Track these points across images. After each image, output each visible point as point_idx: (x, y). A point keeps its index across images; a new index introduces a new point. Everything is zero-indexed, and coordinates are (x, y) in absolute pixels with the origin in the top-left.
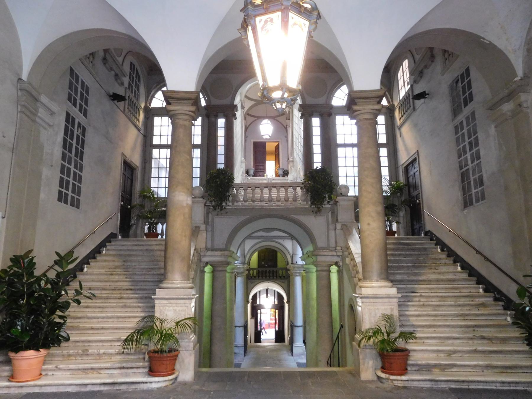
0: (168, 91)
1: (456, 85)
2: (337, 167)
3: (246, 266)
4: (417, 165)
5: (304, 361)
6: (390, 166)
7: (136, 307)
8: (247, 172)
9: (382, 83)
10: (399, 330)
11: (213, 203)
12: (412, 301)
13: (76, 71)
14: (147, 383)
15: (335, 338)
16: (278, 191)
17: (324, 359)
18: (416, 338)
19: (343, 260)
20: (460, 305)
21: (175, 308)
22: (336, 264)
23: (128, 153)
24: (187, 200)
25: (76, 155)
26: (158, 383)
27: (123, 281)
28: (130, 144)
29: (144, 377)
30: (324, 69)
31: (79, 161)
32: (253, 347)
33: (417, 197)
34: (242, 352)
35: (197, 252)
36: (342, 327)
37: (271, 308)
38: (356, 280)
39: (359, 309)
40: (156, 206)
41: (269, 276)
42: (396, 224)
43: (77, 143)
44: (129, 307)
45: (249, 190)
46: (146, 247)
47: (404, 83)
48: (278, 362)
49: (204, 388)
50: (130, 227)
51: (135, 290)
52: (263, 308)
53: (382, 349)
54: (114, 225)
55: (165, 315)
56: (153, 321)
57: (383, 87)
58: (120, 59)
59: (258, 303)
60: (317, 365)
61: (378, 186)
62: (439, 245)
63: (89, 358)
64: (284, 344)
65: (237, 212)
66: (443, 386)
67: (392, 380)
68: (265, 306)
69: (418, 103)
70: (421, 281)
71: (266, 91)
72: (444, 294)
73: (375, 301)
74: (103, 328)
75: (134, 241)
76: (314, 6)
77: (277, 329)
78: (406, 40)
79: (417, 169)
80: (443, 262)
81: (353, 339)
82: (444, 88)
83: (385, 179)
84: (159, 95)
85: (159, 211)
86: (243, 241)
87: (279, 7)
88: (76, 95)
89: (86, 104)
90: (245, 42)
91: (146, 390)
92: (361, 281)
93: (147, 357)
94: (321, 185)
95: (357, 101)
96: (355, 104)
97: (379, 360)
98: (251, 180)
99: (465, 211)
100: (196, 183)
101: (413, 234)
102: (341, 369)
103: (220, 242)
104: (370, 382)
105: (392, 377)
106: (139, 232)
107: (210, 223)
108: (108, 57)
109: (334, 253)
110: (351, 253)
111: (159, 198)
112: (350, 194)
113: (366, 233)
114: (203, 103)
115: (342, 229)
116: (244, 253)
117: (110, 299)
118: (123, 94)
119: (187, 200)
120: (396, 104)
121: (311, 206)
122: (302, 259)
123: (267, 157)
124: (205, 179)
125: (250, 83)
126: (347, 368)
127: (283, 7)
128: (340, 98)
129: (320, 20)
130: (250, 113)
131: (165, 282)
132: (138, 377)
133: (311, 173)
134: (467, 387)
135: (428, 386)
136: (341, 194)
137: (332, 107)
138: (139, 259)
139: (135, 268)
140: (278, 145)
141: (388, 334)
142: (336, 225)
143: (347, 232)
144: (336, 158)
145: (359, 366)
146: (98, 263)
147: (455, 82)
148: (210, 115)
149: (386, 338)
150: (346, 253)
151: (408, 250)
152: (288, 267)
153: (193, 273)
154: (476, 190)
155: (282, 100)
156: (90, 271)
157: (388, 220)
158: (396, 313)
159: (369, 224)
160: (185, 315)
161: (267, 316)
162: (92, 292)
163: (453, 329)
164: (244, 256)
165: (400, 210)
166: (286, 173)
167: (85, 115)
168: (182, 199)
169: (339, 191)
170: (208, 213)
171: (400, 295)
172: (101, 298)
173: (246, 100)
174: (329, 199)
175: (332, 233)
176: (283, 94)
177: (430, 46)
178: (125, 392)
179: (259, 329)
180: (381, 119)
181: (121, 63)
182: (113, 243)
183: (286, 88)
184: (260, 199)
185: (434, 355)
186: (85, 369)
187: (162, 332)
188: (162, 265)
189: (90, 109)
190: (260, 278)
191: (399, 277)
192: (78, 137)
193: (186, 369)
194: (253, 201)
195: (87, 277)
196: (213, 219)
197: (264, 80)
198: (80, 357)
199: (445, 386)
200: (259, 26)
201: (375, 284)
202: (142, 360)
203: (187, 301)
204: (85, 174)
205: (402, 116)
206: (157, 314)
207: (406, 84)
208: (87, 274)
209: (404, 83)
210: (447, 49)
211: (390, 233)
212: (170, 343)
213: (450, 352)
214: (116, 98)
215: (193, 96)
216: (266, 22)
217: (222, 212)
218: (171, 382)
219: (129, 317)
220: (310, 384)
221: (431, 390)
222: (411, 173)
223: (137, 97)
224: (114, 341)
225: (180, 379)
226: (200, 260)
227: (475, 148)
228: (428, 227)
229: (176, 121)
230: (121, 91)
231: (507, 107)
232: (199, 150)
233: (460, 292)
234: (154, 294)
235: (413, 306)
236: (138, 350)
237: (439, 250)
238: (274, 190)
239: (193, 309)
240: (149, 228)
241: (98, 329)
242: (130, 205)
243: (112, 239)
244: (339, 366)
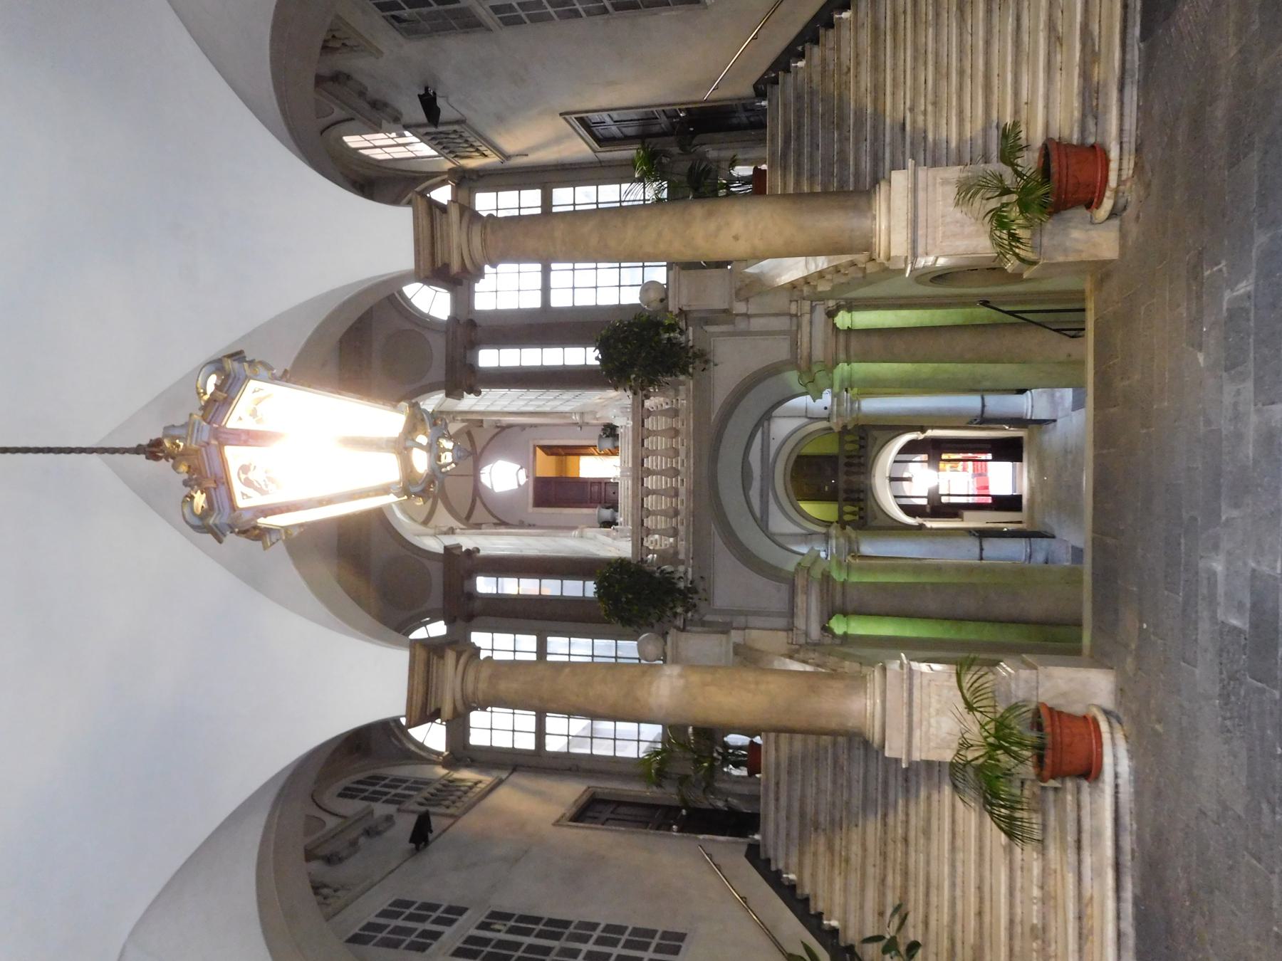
0: (408, 715)
1: (405, 21)
2: (597, 309)
3: (833, 531)
4: (595, 117)
5: (1068, 394)
6: (597, 181)
7: (929, 805)
8: (608, 524)
9: (395, 201)
10: (996, 166)
11: (679, 610)
12: (925, 132)
13: (356, 930)
14: (1117, 786)
15: (1012, 319)
16: (654, 453)
17: (1067, 346)
18: (1016, 124)
19: (822, 298)
20: (937, 15)
21: (932, 711)
22: (831, 314)
23: (556, 811)
24: (670, 676)
25: (557, 936)
26: (1117, 759)
27: (864, 832)
28: (534, 805)
29: (1103, 791)
30: (366, 345)
31: (571, 929)
32: (1031, 517)
33: (672, 115)
34: (1044, 543)
35: (797, 651)
36: (985, 303)
37: (938, 470)
38: (871, 268)
39: (942, 262)
40: (684, 746)
42: (737, 168)
43: (527, 932)
44: (928, 821)
45: (650, 502)
46: (784, 777)
47: (398, 145)
48: (1070, 457)
49: (1133, 646)
50: (732, 812)
51: (886, 806)
52: (937, 488)
53: (1043, 206)
54: (728, 849)
55: (949, 737)
56: (964, 765)
57: (405, 200)
58: (331, 822)
59: (924, 502)
60: (1081, 363)
61: (644, 214)
62: (789, 66)
63: (1053, 923)
64: (1025, 440)
65: (700, 552)
66: (1135, 56)
67: (1120, 182)
68: (932, 484)
69: (446, 113)
70: (875, 109)
71: (410, 486)
72: (909, 53)
73: (924, 222)
74: (980, 888)
75: (766, 804)
76: (212, 367)
77: (989, 456)
78: (298, 146)
79: (605, 116)
80: (829, 54)
81: (1017, 277)
82: (414, 49)
83: (627, 193)
84: (418, 733)
85: (694, 744)
86: (771, 537)
87: (214, 451)
88: (412, 931)
90: (295, 533)
91: (1135, 788)
92: (875, 256)
93: (1052, 783)
94: (639, 349)
96: (446, 266)
97: (1068, 214)
98: (624, 515)
100: (629, 648)
102: (1090, 306)
103: (773, 595)
104: (1123, 235)
105: (1113, 181)
106: (745, 790)
107: (728, 619)
108: (326, 850)
109: (806, 318)
110: (806, 280)
111: (665, 739)
112: (663, 280)
114: (438, 629)
115: (747, 300)
116: (802, 535)
118: (413, 819)
119: (670, 676)
120: (448, 165)
121: (691, 375)
122: (817, 396)
123: (571, 474)
124: (618, 627)
126: (1088, 293)
127: (214, 442)
128: (433, 302)
129: (246, 354)
130: (464, 516)
131: (868, 735)
132: (1102, 806)
133: (610, 374)
135: (1135, 93)
136: (662, 300)
137: (453, 319)
138: (811, 792)
139: (834, 804)
140: (543, 448)
141: (1006, 191)
143: (753, 288)
144: (574, 310)
145: (1082, 262)
146: (820, 892)
147: (396, 24)
148: (470, 612)
149: (1014, 197)
150: (806, 289)
151: (799, 138)
152: (837, 429)
153: (847, 663)
155: (434, 450)
156: (837, 911)
157: (727, 187)
158: (954, 173)
159: (736, 238)
160: (950, 688)
161: (955, 480)
162: (889, 911)
163: (996, 30)
164: (807, 537)
165: (703, 157)
166: (610, 431)
167: (461, 911)
168: (667, 687)
169: (656, 305)
170: (703, 624)
171: (910, 162)
172: (905, 889)
173: (432, 523)
174: (674, 331)
175: (756, 324)
176: (420, 446)
177: (312, 80)
178: (1140, 839)
179: (989, 500)
180: (485, 202)
181: (340, 820)
182: (771, 854)
183: (406, 439)
184: (671, 497)
185: (1059, 79)
187: (990, 744)
188: (826, 740)
189: (446, 900)
191: (866, 164)
192: (512, 931)
193: (1085, 687)
194: (676, 513)
195: (853, 920)
196: (721, 612)
197: (385, 490)
199: (1136, 52)
200: (256, 500)
201: (881, 223)
202: (1060, 795)
203: (916, 681)
204: (603, 917)
205: (477, 150)
206: (948, 756)
207: (401, 140)
208: (845, 921)
209: (398, 145)
210: (320, 44)
211: (758, 183)
212: (1020, 727)
213: (1053, 39)
214: (421, 835)
215: (421, 654)
216: (248, 483)
217: (700, 589)
218: (1116, 725)
219: (953, 822)
220: (1126, 383)
221: (1145, 87)
222: (614, 130)
223: (419, 784)
225: (1108, 703)
226: (816, 646)
228: (744, 88)
229: (480, 696)
230: (406, 824)
232: (549, 639)
233: (905, 12)
234: (897, 761)
235: (936, 126)
236: (1034, 805)
237: (801, 64)
238: (649, 463)
239: (936, 667)
240: (737, 766)
241: (981, 900)
242: (679, 809)
243: (763, 856)
244: (1083, 310)
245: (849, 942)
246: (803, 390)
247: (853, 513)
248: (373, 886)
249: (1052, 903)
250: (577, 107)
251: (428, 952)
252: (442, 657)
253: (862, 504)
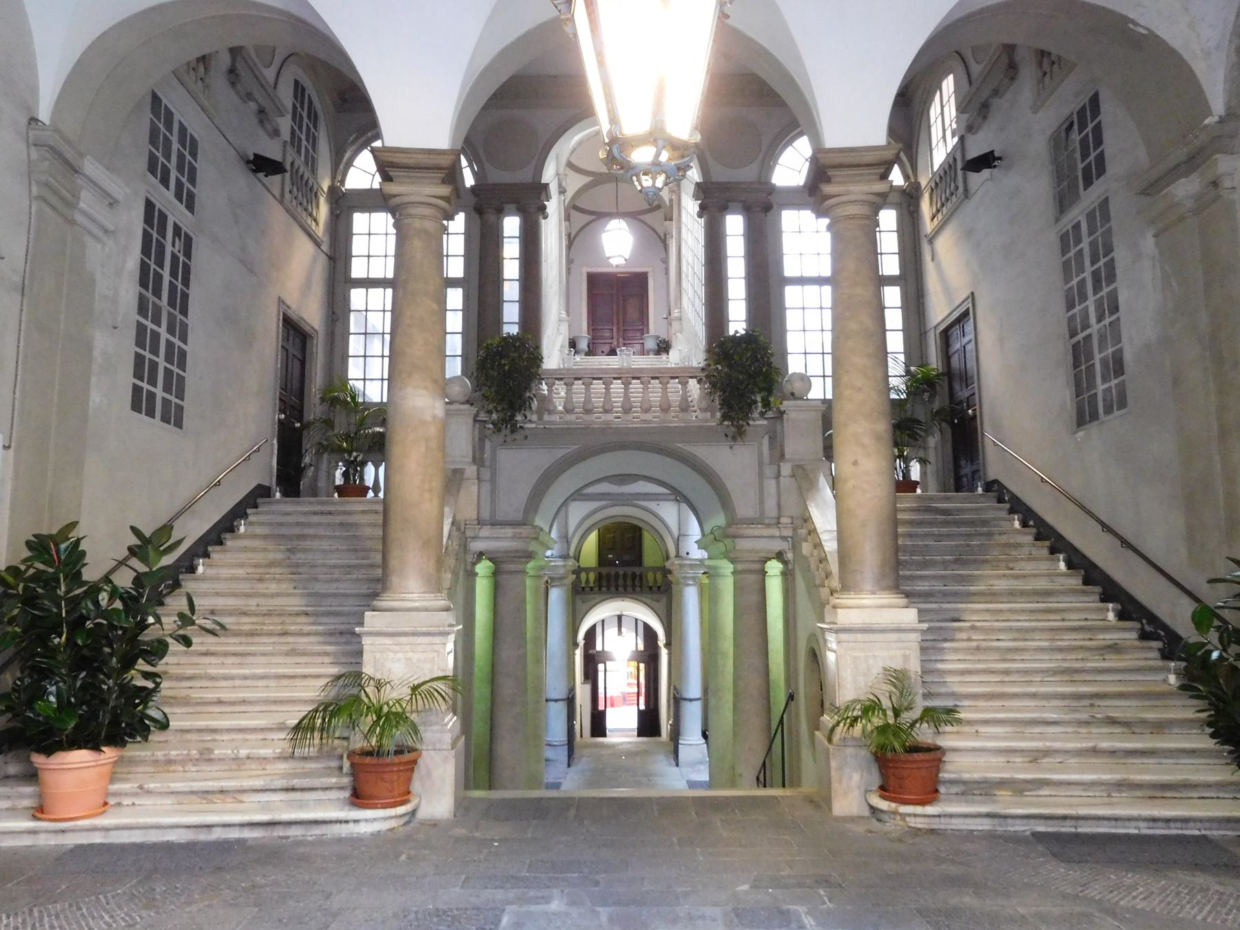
4: (969, 327)
14: (347, 822)
21: (410, 655)
25: (172, 303)
26: (372, 821)
31: (180, 317)
41: (625, 587)
43: (174, 274)
59: (599, 647)
95: (831, 173)
96: (828, 180)
99: (1081, 434)
107: (487, 463)
109: (776, 532)
113: (849, 485)
118: (277, 157)
120: (923, 182)
122: (701, 545)
134: (1073, 830)
136: (793, 394)
142: (779, 466)
144: (782, 309)
154: (1106, 386)
159: (855, 463)
167: (190, 207)
175: (770, 485)
186: (207, 792)
190: (604, 589)
198: (194, 765)
215: (445, 161)
219: (305, 677)
222: (956, 346)
224: (271, 729)
231: (1185, 189)
246: (707, 530)
247: (587, 581)
249: (235, 767)
253: (596, 589)
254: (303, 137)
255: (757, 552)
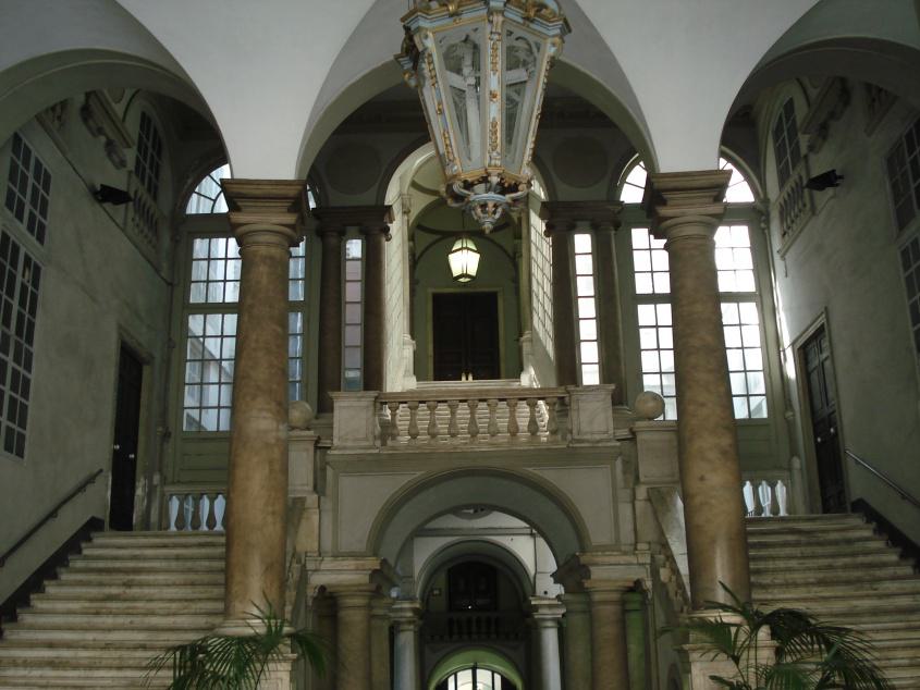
4: (825, 344)
24: (278, 430)
25: (19, 332)
31: (25, 345)
43: (22, 303)
45: (443, 411)
84: (210, 186)
89: (44, 213)
95: (666, 196)
96: (664, 203)
101: (826, 510)
109: (632, 559)
113: (698, 500)
117: (98, 668)
118: (123, 188)
119: (278, 430)
125: (426, 152)
159: (702, 479)
167: (41, 239)
173: (413, 191)
175: (625, 510)
215: (292, 191)
222: (815, 363)
227: (916, 301)
232: (191, 301)
245: (20, 618)
248: (62, 152)
250: (834, 325)
251: (6, 209)
252: (290, 210)
254: (147, 166)
255: (616, 581)
